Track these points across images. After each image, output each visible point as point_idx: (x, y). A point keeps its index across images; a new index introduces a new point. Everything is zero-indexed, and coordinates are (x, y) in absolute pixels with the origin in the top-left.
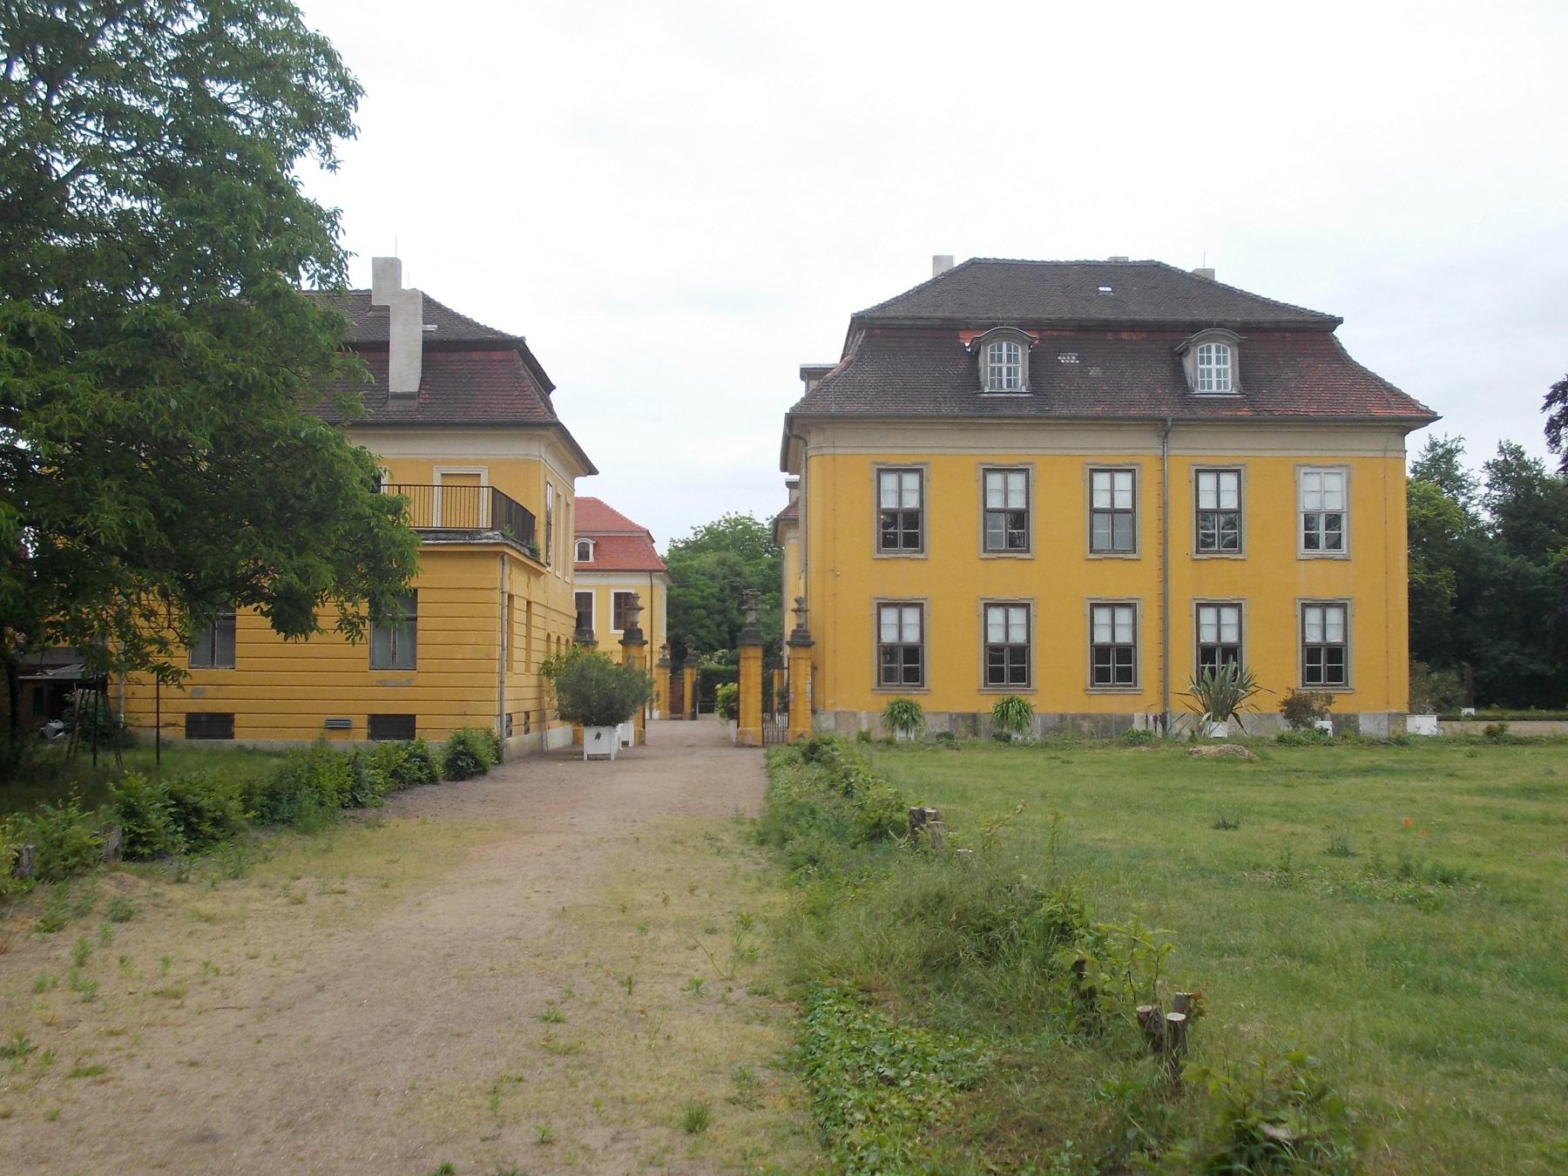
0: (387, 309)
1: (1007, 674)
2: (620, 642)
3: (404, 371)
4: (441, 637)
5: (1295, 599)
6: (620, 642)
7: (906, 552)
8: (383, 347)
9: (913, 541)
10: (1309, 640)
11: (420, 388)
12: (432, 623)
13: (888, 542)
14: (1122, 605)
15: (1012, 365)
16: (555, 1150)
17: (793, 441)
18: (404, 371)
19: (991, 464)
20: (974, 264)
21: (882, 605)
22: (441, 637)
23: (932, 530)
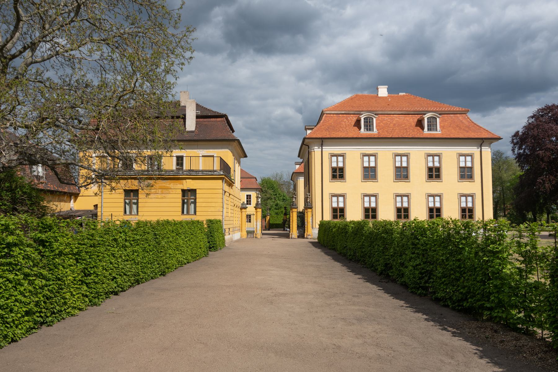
0: (185, 107)
1: (403, 216)
2: (254, 207)
3: (191, 124)
4: (204, 205)
5: (458, 194)
6: (254, 207)
7: (339, 180)
8: (184, 118)
9: (438, 176)
10: (365, 206)
11: (195, 130)
12: (201, 200)
13: (430, 177)
14: (469, 196)
15: (429, 124)
16: (499, 340)
17: (304, 146)
18: (191, 124)
19: (365, 153)
20: (388, 91)
21: (397, 196)
22: (204, 205)
23: (444, 173)
